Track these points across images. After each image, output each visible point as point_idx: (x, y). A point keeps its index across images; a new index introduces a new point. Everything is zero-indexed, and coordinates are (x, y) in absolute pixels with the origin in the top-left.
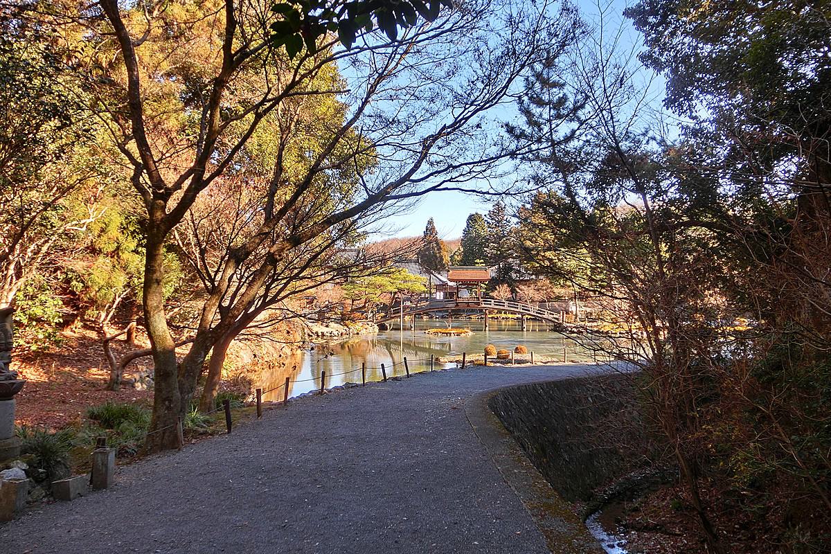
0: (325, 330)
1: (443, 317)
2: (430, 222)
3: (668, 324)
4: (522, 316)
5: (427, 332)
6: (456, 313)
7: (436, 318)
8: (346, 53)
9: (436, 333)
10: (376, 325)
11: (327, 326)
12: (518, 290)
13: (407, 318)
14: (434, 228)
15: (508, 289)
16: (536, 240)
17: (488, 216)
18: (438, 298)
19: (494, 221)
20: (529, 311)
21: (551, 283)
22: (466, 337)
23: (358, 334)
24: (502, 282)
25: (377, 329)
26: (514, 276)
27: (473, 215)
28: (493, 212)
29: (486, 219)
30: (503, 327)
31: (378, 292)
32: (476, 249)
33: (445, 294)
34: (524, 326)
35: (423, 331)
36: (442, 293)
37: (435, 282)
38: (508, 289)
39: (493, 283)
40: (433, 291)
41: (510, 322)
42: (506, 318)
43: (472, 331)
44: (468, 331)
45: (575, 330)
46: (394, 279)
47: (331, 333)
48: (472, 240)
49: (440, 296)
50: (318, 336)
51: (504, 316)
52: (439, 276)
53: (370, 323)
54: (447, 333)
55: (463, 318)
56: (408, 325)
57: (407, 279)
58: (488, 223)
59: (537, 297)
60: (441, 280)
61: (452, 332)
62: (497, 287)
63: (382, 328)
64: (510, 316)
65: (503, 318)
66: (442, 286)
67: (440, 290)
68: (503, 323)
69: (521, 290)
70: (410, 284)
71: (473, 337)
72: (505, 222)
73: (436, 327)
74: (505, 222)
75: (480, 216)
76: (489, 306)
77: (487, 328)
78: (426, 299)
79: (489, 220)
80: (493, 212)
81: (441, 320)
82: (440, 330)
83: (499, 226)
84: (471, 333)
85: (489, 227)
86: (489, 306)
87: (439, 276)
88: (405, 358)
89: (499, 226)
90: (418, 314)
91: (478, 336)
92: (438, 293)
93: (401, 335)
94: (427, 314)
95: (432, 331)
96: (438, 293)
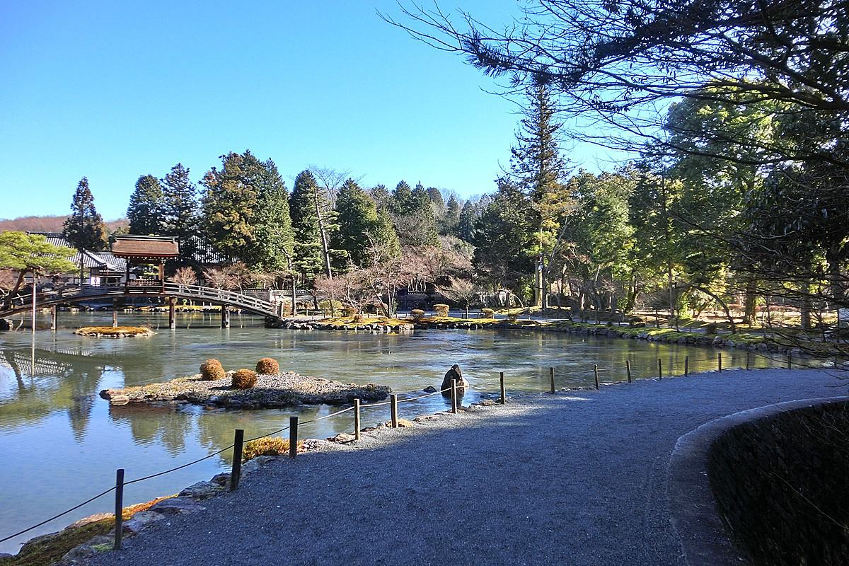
1: (100, 310)
2: (83, 184)
3: (812, 279)
5: (77, 331)
6: (119, 305)
7: (91, 311)
9: (92, 334)
12: (208, 276)
13: (46, 311)
14: (88, 192)
16: (230, 213)
17: (165, 181)
19: (172, 188)
21: (247, 267)
22: (144, 339)
24: (185, 265)
26: (198, 257)
28: (173, 176)
29: (162, 184)
30: (185, 322)
32: (148, 223)
33: (103, 280)
34: (228, 320)
35: (71, 331)
37: (88, 263)
39: (172, 266)
40: (86, 275)
42: (190, 310)
44: (146, 329)
45: (297, 325)
48: (145, 209)
49: (95, 281)
54: (111, 334)
55: (128, 311)
56: (47, 320)
57: (45, 251)
58: (165, 189)
59: (231, 284)
60: (96, 261)
62: (178, 271)
64: (195, 307)
65: (185, 311)
66: (98, 270)
67: (95, 275)
68: (185, 316)
69: (210, 275)
71: (153, 338)
72: (188, 189)
73: (94, 325)
74: (188, 189)
75: (154, 180)
76: (177, 293)
77: (174, 326)
80: (173, 176)
81: (97, 313)
82: (100, 328)
84: (150, 333)
85: (166, 195)
86: (177, 293)
88: (239, 434)
90: (62, 305)
91: (163, 336)
94: (76, 305)
95: (86, 330)
96: (93, 279)
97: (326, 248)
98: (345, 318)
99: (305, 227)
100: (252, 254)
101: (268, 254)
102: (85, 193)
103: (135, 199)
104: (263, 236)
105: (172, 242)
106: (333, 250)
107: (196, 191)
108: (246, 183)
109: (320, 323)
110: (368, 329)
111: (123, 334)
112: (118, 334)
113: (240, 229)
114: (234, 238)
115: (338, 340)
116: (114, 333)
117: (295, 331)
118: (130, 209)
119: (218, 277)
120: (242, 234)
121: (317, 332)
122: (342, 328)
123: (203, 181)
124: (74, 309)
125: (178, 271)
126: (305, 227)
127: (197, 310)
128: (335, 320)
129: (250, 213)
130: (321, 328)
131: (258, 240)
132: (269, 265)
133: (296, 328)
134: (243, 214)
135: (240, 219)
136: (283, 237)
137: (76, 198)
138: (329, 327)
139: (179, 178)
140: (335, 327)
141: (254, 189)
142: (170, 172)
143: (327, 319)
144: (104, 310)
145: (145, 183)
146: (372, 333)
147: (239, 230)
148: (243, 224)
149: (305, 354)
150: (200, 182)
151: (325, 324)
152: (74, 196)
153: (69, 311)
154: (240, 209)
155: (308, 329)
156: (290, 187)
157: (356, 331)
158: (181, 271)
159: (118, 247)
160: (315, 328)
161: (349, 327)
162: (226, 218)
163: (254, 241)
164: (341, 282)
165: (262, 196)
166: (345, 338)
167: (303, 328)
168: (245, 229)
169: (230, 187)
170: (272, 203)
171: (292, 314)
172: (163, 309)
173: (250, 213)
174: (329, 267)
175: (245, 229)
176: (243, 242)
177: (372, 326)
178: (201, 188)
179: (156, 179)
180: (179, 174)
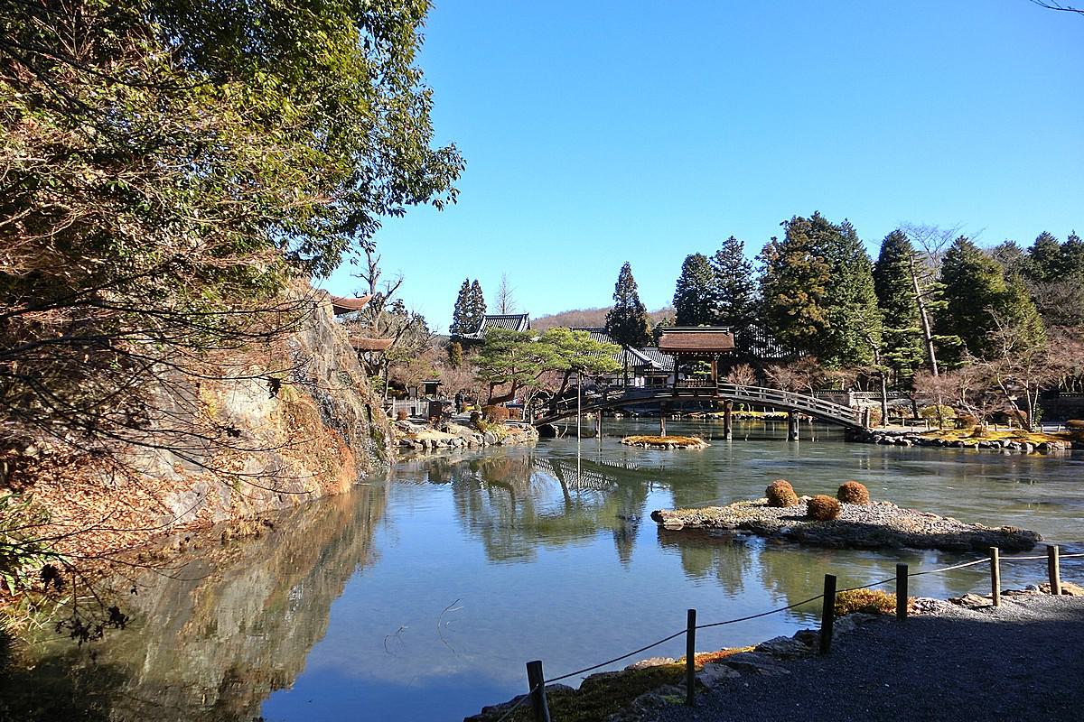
0: (438, 435)
2: (626, 269)
4: (790, 413)
5: (623, 441)
6: (665, 410)
7: (635, 417)
8: (625, 404)
10: (534, 429)
11: (444, 430)
14: (631, 279)
15: (751, 371)
16: (795, 293)
17: (716, 260)
18: (637, 385)
19: (723, 267)
20: (781, 399)
21: (818, 362)
23: (499, 444)
24: (741, 361)
25: (535, 436)
27: (700, 256)
31: (537, 368)
36: (643, 379)
38: (751, 371)
39: (727, 362)
40: (630, 375)
41: (755, 424)
43: (706, 439)
44: (698, 439)
45: (891, 439)
46: (566, 349)
47: (449, 443)
49: (639, 382)
50: (425, 447)
51: (744, 414)
52: (640, 354)
53: (524, 425)
54: (660, 445)
56: (591, 427)
58: (716, 269)
59: (798, 384)
60: (641, 359)
61: (670, 442)
62: (733, 369)
63: (546, 433)
64: (754, 414)
65: (743, 418)
66: (643, 368)
68: (743, 425)
69: (773, 373)
70: (593, 357)
72: (742, 268)
74: (742, 268)
75: (703, 259)
78: (618, 388)
79: (717, 266)
80: (724, 252)
81: (643, 420)
83: (732, 274)
84: (703, 445)
85: (717, 276)
87: (640, 354)
89: (732, 274)
90: (607, 408)
91: (718, 449)
92: (637, 379)
93: (579, 447)
95: (633, 439)
96: (637, 379)
97: (929, 334)
98: (960, 431)
99: (897, 306)
100: (825, 345)
101: (846, 344)
102: (627, 280)
103: (682, 284)
104: (839, 320)
105: (726, 333)
106: (938, 337)
107: (753, 269)
108: (815, 254)
109: (923, 437)
110: (996, 446)
111: (673, 444)
112: (667, 445)
113: (809, 313)
114: (801, 325)
115: (951, 460)
116: (664, 444)
117: (887, 447)
118: (676, 296)
119: (783, 375)
120: (812, 320)
121: (919, 449)
122: (955, 444)
123: (762, 256)
124: (618, 415)
125: (733, 369)
126: (897, 306)
127: (757, 418)
128: (945, 433)
129: (822, 293)
130: (924, 443)
131: (833, 327)
132: (849, 359)
133: (888, 443)
134: (813, 294)
135: (810, 301)
136: (867, 321)
137: (618, 287)
138: (935, 443)
139: (732, 254)
140: (945, 443)
141: (826, 261)
142: (721, 248)
143: (932, 431)
144: (650, 416)
145: (693, 264)
146: (1002, 452)
147: (807, 315)
148: (813, 308)
149: (903, 479)
150: (757, 258)
151: (930, 438)
152: (616, 284)
153: (613, 416)
154: (809, 287)
155: (905, 444)
156: (874, 253)
157: (977, 449)
158: (736, 369)
159: (666, 342)
160: (916, 443)
161: (966, 443)
162: (791, 301)
163: (827, 329)
164: (952, 380)
165: (837, 269)
166: (960, 458)
167: (898, 443)
168: (815, 312)
169: (794, 261)
170: (851, 277)
171: (882, 424)
172: (716, 415)
173: (822, 293)
174: (934, 361)
175: (815, 312)
176: (813, 329)
177: (1002, 443)
178: (759, 264)
179: (705, 257)
180: (732, 248)
